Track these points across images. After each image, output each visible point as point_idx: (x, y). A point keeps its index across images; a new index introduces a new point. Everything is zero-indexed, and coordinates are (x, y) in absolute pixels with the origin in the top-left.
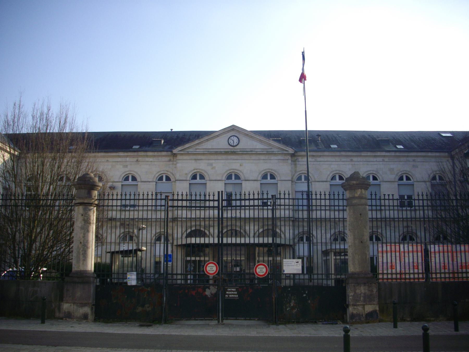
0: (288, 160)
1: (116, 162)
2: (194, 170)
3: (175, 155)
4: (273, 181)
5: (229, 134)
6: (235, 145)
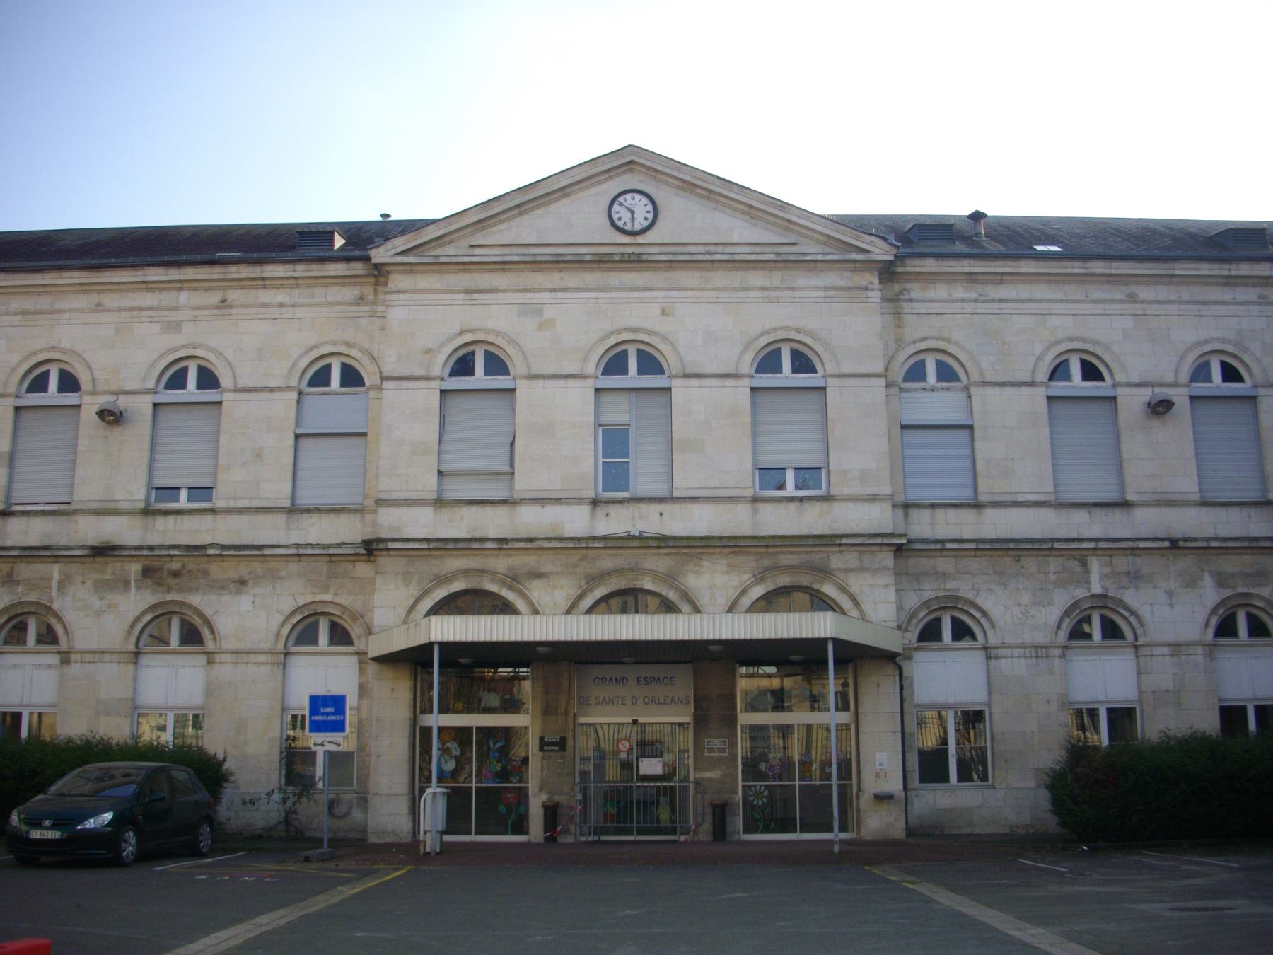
0: (866, 289)
1: (132, 309)
2: (462, 333)
3: (379, 273)
4: (804, 379)
5: (613, 187)
6: (637, 227)
